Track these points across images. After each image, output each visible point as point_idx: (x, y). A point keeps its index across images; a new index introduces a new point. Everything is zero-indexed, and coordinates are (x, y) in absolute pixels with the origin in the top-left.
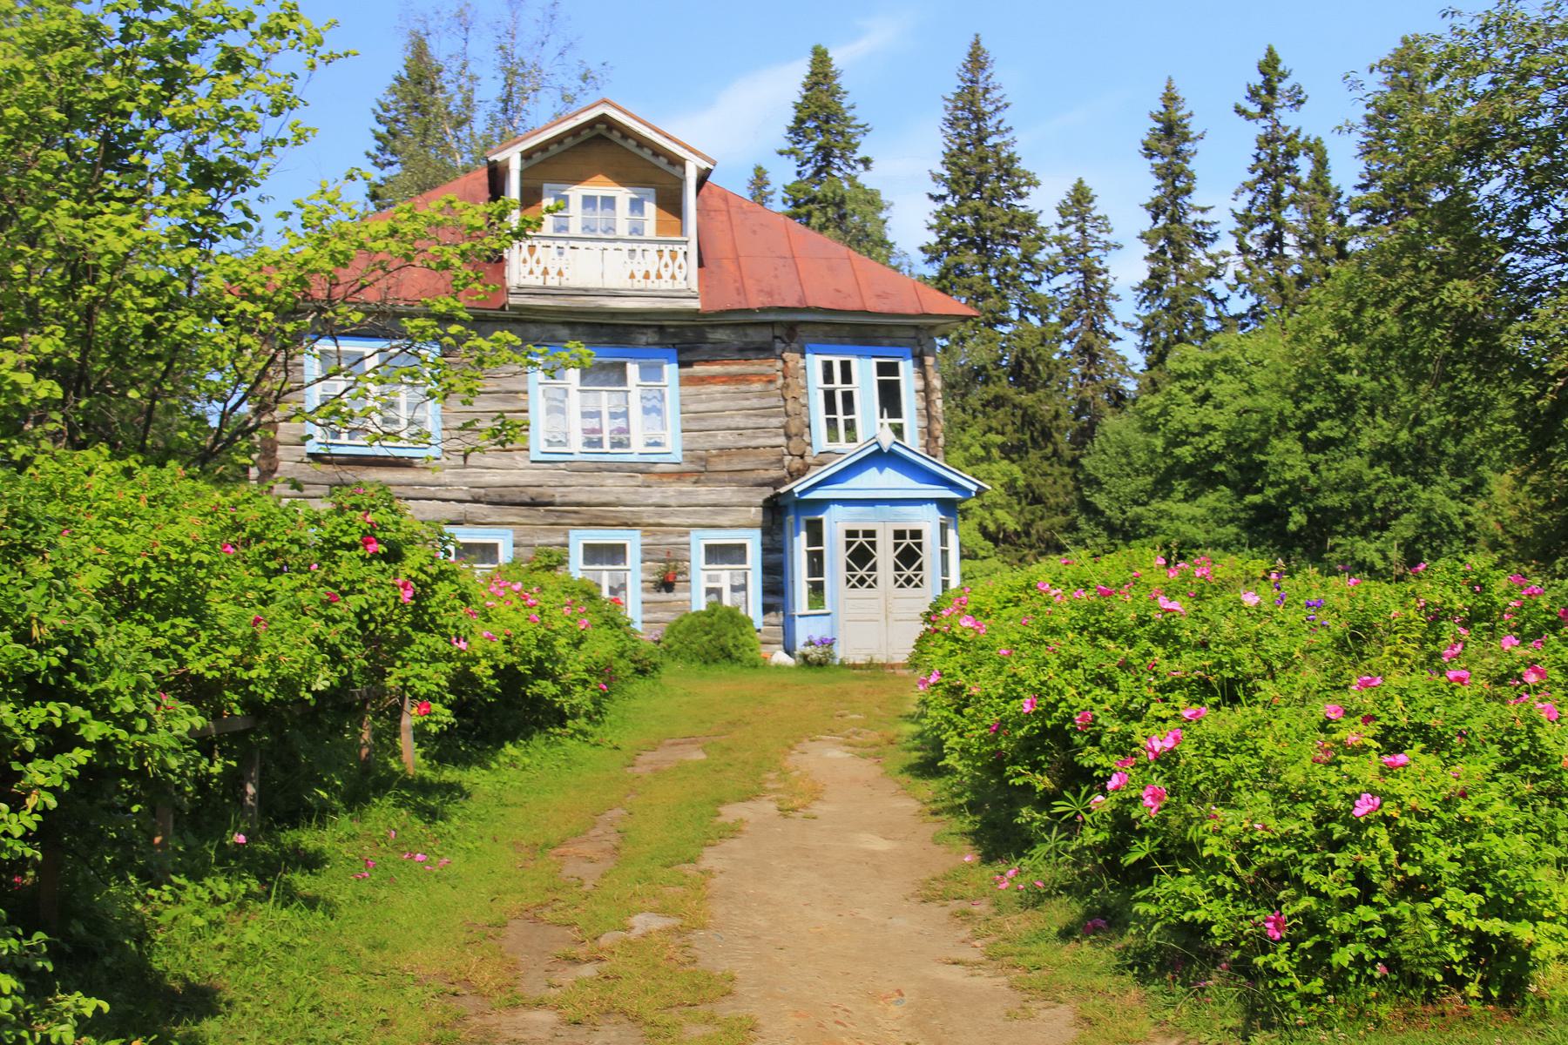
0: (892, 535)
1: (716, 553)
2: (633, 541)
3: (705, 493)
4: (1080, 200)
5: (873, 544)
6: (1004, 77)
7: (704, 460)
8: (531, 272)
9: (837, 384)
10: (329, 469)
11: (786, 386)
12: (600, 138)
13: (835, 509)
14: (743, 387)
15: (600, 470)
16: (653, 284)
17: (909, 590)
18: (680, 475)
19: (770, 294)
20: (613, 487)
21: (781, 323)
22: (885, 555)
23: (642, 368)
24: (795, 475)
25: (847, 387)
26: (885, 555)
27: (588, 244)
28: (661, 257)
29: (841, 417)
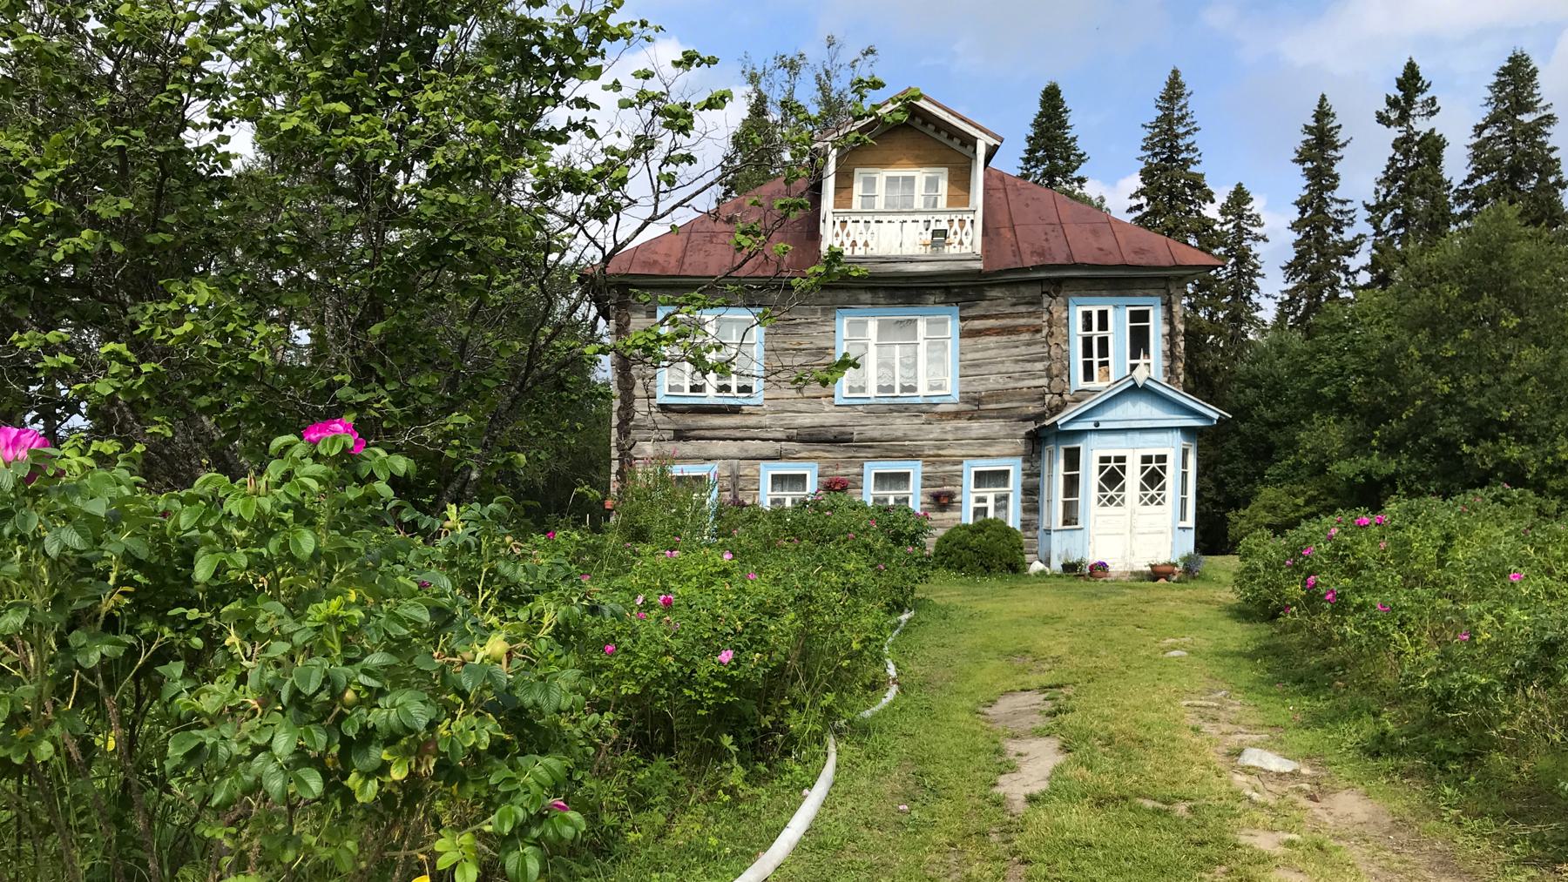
0: (1139, 460)
1: (982, 478)
3: (977, 428)
4: (1240, 197)
5: (1123, 469)
6: (1196, 105)
7: (978, 401)
9: (1096, 332)
10: (675, 417)
11: (1051, 334)
13: (1093, 439)
14: (1014, 338)
15: (891, 411)
17: (1153, 507)
18: (957, 415)
19: (1041, 254)
20: (900, 425)
22: (1133, 476)
23: (928, 323)
24: (1058, 409)
25: (1103, 334)
26: (1133, 476)
27: (891, 218)
29: (1096, 360)
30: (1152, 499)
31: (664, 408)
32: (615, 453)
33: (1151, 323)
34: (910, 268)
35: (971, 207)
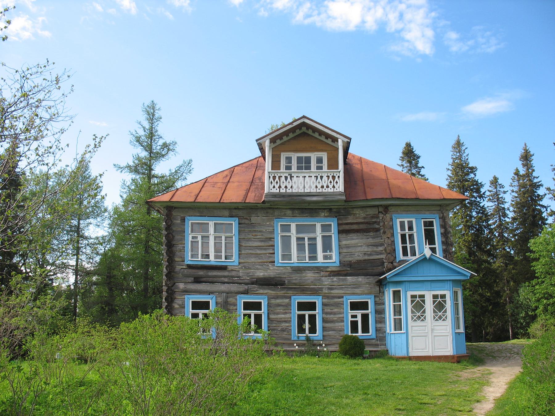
1: (355, 306)
2: (318, 301)
4: (495, 182)
8: (274, 187)
12: (304, 134)
16: (325, 190)
21: (381, 205)
22: (429, 305)
25: (411, 232)
26: (429, 305)
28: (317, 179)
30: (440, 318)
31: (190, 267)
32: (165, 288)
33: (435, 228)
34: (309, 199)
35: (339, 170)
